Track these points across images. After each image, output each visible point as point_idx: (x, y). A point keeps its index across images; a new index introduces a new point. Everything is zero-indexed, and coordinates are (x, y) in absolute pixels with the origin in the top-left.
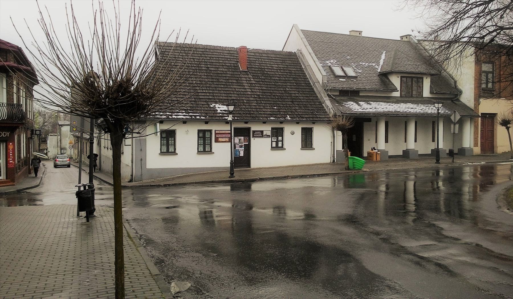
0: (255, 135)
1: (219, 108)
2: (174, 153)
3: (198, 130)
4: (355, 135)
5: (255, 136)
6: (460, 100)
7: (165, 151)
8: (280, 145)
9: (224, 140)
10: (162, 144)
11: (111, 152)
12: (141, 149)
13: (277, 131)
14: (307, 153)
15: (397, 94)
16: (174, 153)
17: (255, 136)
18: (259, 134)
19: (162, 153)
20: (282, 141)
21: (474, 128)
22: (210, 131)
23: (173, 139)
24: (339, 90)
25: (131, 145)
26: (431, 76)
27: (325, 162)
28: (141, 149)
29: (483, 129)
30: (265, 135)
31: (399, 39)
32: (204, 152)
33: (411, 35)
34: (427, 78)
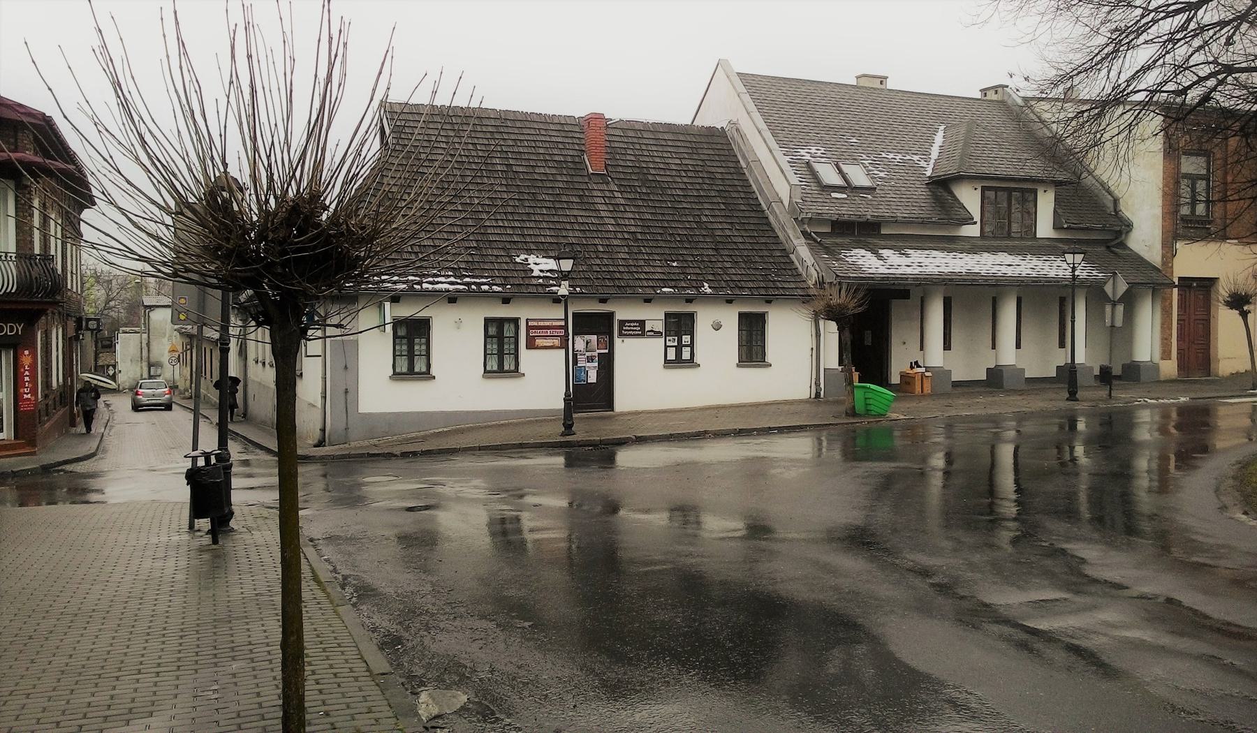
0: (625, 330)
1: (536, 264)
2: (427, 375)
3: (485, 319)
4: (869, 332)
5: (626, 333)
6: (1126, 246)
7: (405, 370)
8: (686, 354)
9: (550, 343)
10: (397, 353)
11: (272, 372)
12: (346, 366)
13: (679, 321)
14: (753, 374)
15: (973, 231)
16: (427, 375)
17: (626, 333)
18: (635, 328)
19: (397, 375)
20: (692, 345)
21: (1162, 314)
22: (515, 321)
23: (423, 340)
24: (830, 222)
25: (320, 356)
26: (1056, 186)
27: (797, 397)
28: (346, 366)
29: (1183, 317)
30: (648, 331)
31: (978, 95)
32: (501, 372)
33: (1007, 87)
34: (1045, 191)
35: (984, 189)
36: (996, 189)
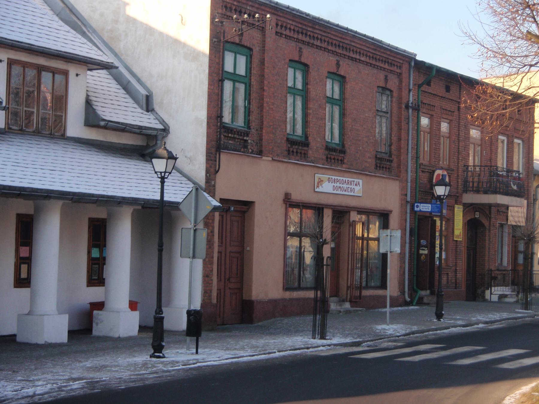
34: (77, 75)
35: (11, 63)
36: (25, 65)
